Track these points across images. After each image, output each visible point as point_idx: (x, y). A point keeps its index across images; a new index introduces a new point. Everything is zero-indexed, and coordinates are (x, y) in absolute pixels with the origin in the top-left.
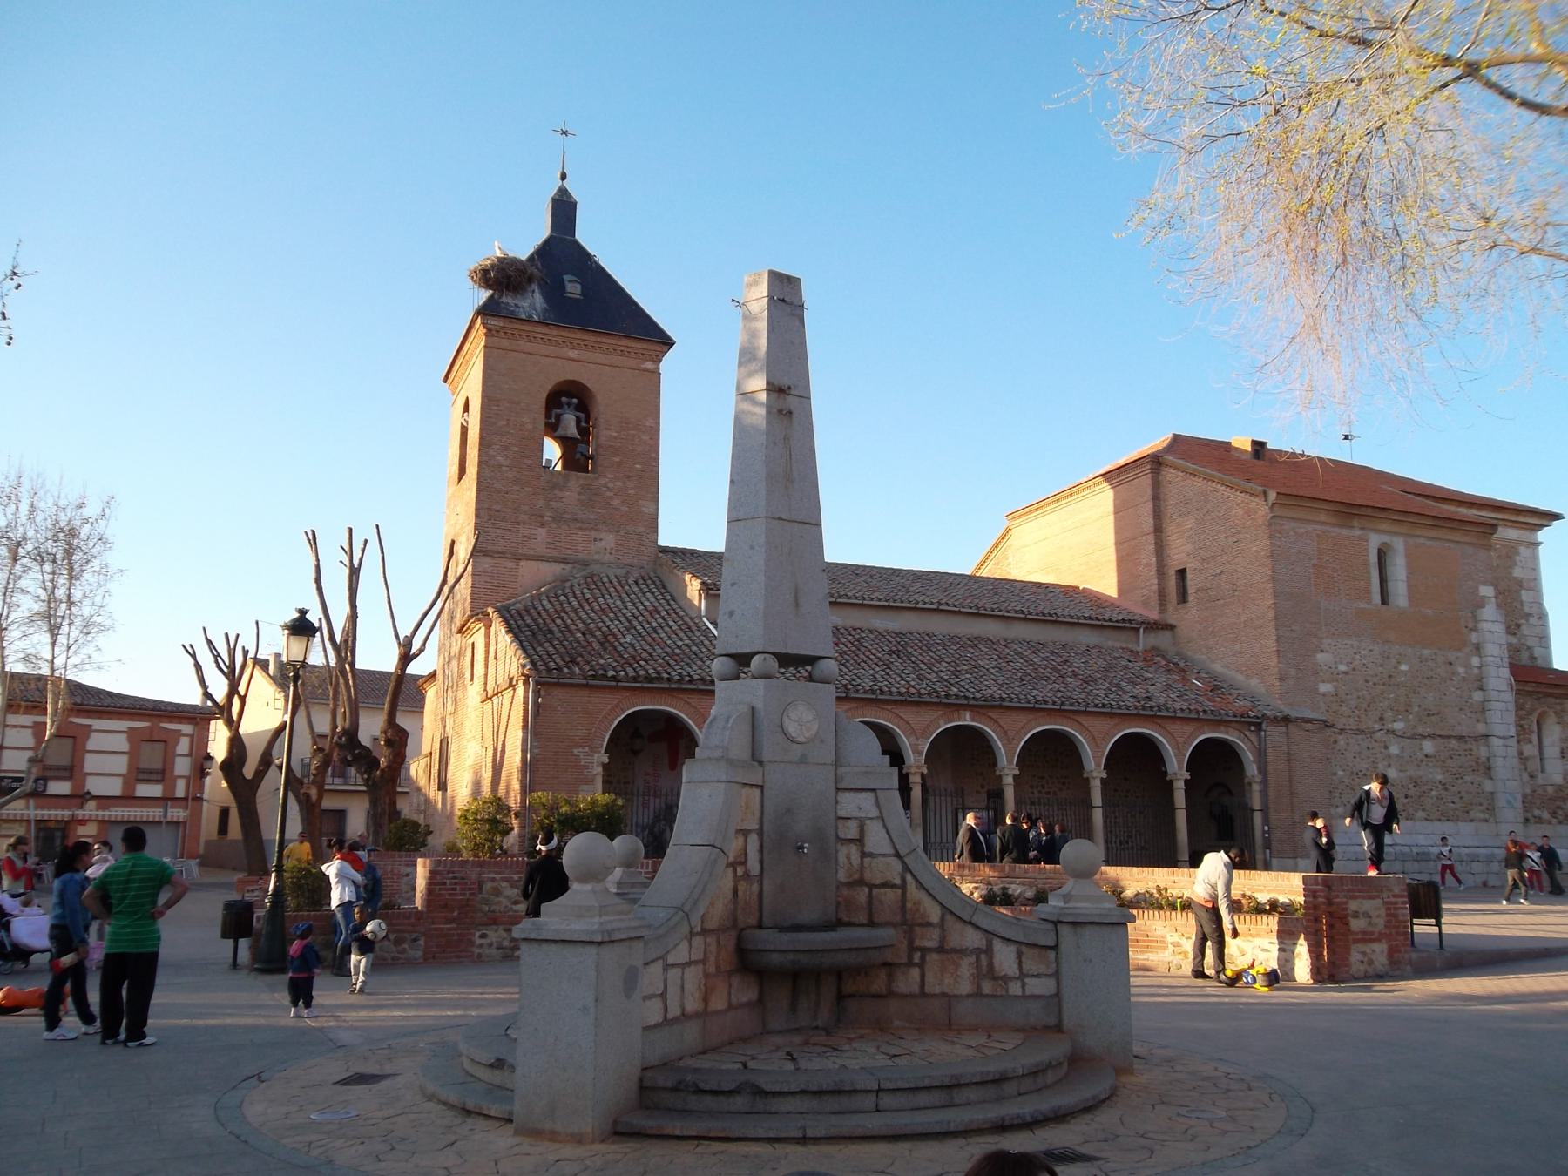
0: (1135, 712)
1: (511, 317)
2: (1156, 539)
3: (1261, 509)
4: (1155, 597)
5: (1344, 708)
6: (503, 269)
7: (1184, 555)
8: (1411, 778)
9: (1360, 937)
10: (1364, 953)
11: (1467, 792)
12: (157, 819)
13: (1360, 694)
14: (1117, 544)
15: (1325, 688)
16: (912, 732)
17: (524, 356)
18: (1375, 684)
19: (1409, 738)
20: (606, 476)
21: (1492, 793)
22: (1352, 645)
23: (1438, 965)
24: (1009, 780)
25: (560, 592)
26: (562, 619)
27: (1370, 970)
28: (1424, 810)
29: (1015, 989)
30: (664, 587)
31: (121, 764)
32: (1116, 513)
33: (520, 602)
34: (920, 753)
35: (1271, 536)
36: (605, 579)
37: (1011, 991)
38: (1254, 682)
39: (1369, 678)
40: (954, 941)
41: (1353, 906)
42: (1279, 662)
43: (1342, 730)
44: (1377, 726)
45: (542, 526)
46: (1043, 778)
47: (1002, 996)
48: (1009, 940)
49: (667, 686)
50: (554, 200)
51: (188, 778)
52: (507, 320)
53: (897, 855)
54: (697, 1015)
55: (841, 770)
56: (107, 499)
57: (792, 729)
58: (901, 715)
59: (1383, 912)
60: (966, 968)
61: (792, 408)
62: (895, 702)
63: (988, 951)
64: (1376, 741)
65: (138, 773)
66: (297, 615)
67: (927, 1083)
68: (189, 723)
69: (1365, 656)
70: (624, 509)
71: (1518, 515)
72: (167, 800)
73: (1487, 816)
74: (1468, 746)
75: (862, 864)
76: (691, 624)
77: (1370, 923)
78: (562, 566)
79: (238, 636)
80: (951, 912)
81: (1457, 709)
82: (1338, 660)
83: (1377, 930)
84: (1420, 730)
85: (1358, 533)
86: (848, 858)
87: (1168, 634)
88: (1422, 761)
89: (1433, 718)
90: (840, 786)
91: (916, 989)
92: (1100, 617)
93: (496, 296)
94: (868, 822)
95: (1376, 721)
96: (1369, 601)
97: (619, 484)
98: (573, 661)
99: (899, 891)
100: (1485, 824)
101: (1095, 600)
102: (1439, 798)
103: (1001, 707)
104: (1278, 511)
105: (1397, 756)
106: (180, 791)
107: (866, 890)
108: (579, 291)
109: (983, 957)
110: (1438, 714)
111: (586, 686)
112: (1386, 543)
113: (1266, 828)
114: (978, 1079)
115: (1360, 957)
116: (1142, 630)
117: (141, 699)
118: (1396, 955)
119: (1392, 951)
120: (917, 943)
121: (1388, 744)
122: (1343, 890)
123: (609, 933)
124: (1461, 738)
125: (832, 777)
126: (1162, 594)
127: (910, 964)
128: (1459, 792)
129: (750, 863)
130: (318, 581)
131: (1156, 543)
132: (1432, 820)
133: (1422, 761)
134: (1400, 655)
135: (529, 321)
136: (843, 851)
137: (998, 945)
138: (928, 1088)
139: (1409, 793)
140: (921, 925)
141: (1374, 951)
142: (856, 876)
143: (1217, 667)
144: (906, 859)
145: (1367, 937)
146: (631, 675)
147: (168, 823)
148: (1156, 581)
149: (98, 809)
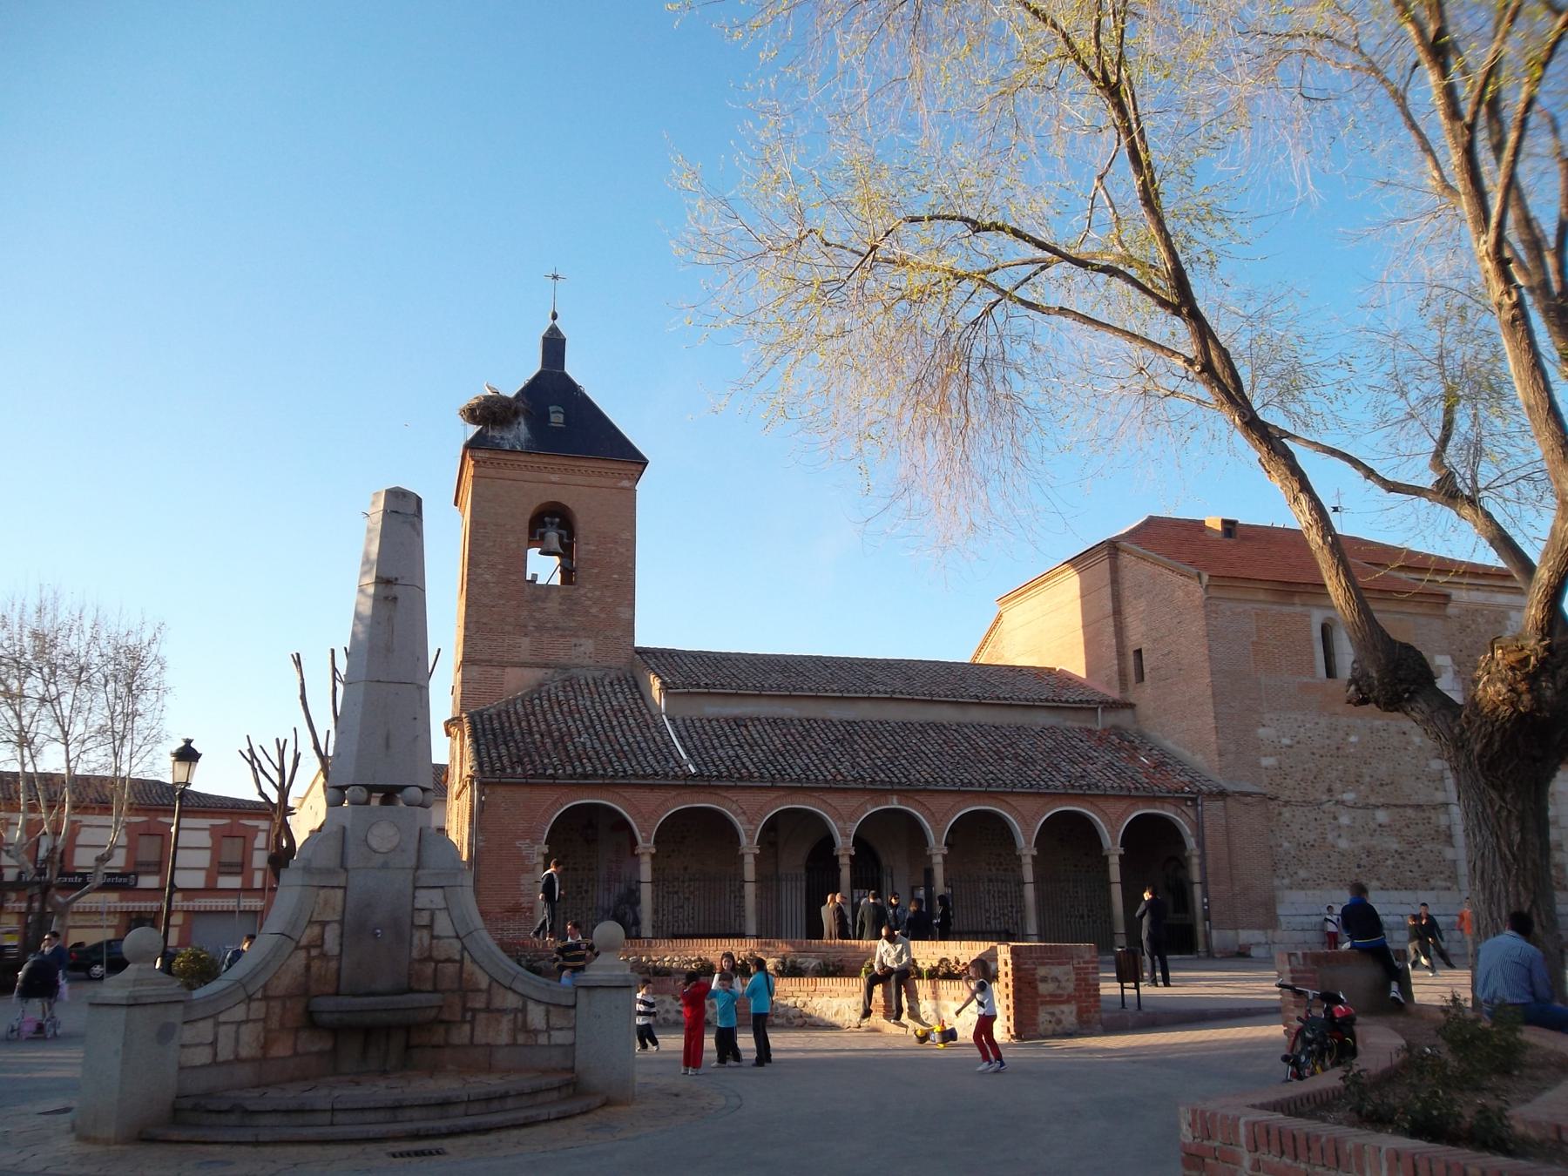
0: (1063, 791)
1: (496, 448)
2: (1115, 621)
3: (1197, 591)
4: (1116, 677)
5: (1288, 781)
6: (488, 407)
7: (1139, 636)
8: (1363, 847)
9: (1048, 999)
10: (1052, 1014)
11: (1426, 861)
12: (231, 909)
13: (1306, 766)
14: (1084, 627)
15: (1267, 762)
16: (839, 817)
17: (510, 482)
18: (1322, 756)
19: (1360, 808)
20: (584, 587)
21: (1455, 861)
22: (1296, 720)
23: (1130, 1024)
24: (938, 859)
25: (536, 696)
26: (528, 721)
27: (1058, 1029)
28: (1378, 879)
29: (543, 1039)
30: (637, 686)
31: (204, 859)
32: (1082, 596)
33: (494, 707)
34: (848, 836)
35: (1207, 617)
36: (582, 682)
37: (539, 1041)
38: (1199, 758)
39: (1315, 751)
40: (497, 1003)
41: (1042, 971)
42: (1218, 738)
43: (1287, 803)
44: (1325, 798)
45: (526, 635)
46: (1000, 855)
47: (531, 1045)
48: (539, 1002)
49: (601, 782)
50: (545, 339)
51: (264, 870)
52: (492, 452)
53: (458, 937)
54: (253, 1060)
55: (420, 872)
56: (157, 625)
57: (374, 843)
58: (829, 801)
59: (1073, 977)
60: (506, 1023)
61: (398, 595)
62: (822, 789)
63: (524, 1010)
64: (1324, 812)
65: (220, 867)
66: (182, 744)
67: (372, 1104)
68: (266, 819)
69: (1310, 729)
70: (603, 616)
71: (1504, 580)
72: (247, 890)
73: (1449, 884)
74: (1427, 814)
75: (431, 944)
76: (650, 721)
77: (1059, 987)
78: (545, 670)
79: (286, 741)
80: (497, 981)
81: (1413, 778)
82: (1280, 734)
83: (1066, 993)
84: (1372, 800)
85: (1299, 609)
86: (421, 939)
87: (1127, 713)
88: (1375, 831)
89: (1386, 788)
90: (418, 884)
91: (466, 1041)
92: (1057, 699)
93: (484, 431)
94: (437, 912)
95: (1323, 793)
96: (1313, 675)
97: (598, 593)
98: (520, 762)
99: (458, 965)
100: (1447, 892)
101: (1061, 679)
102: (1396, 866)
103: (925, 790)
104: (1214, 593)
105: (1348, 826)
106: (258, 883)
107: (433, 964)
108: (561, 420)
109: (519, 1015)
110: (1392, 783)
111: (527, 784)
112: (1330, 618)
113: (1206, 900)
114: (421, 1102)
115: (1048, 1018)
116: (1099, 710)
117: (225, 798)
118: (1085, 1016)
119: (1080, 1012)
120: (469, 1005)
121: (1337, 815)
122: (1031, 958)
123: (135, 998)
124: (1418, 807)
125: (411, 877)
126: (1122, 674)
127: (464, 1021)
128: (1418, 861)
129: (326, 947)
130: (303, 697)
131: (1115, 626)
132: (1388, 889)
133: (1375, 831)
134: (1349, 727)
135: (513, 451)
136: (417, 935)
137: (531, 1006)
138: (376, 1109)
139: (1362, 863)
140: (472, 991)
141: (1063, 1012)
142: (426, 955)
143: (1169, 744)
144: (464, 940)
145: (1056, 999)
146: (568, 772)
147: (240, 912)
148: (1116, 662)
149: (121, 900)
